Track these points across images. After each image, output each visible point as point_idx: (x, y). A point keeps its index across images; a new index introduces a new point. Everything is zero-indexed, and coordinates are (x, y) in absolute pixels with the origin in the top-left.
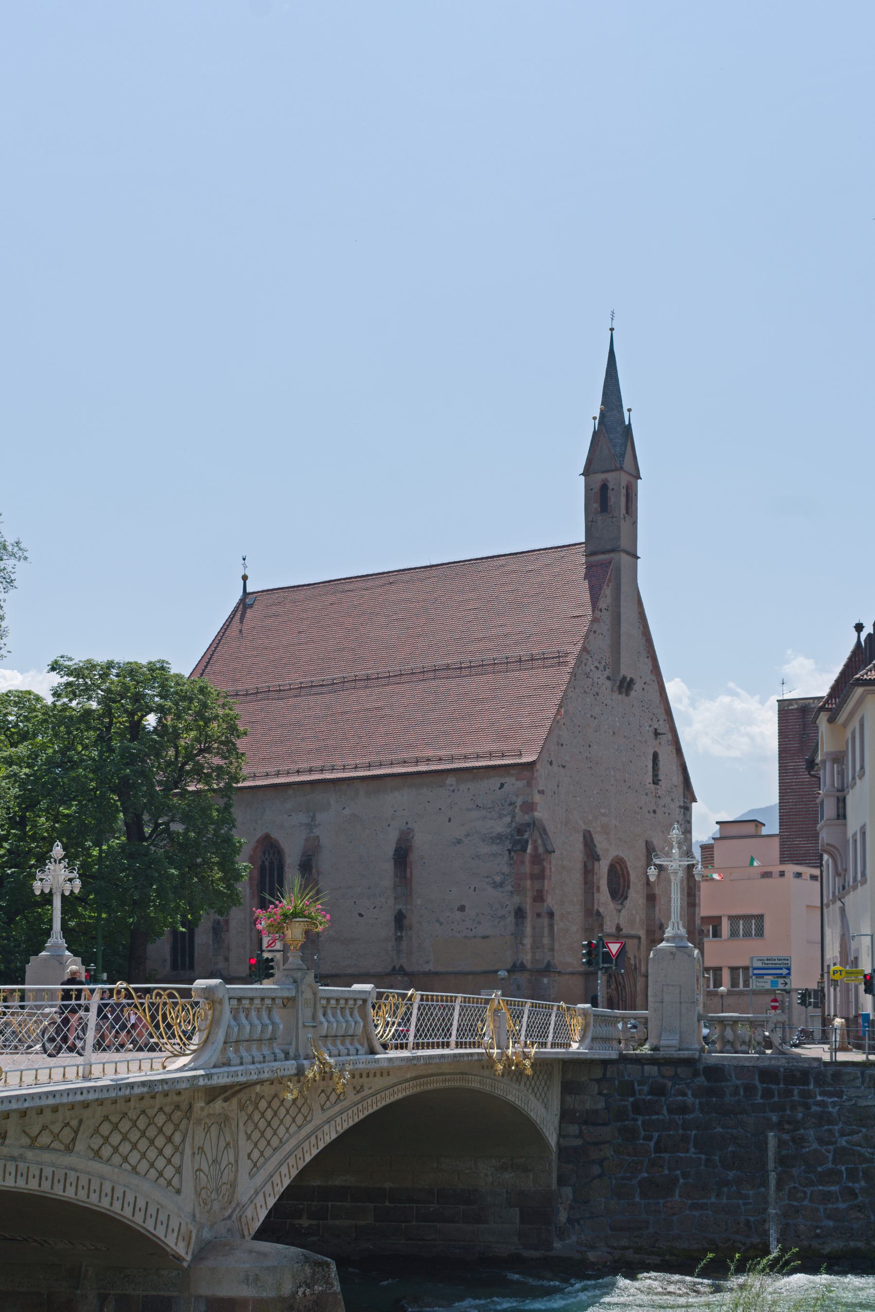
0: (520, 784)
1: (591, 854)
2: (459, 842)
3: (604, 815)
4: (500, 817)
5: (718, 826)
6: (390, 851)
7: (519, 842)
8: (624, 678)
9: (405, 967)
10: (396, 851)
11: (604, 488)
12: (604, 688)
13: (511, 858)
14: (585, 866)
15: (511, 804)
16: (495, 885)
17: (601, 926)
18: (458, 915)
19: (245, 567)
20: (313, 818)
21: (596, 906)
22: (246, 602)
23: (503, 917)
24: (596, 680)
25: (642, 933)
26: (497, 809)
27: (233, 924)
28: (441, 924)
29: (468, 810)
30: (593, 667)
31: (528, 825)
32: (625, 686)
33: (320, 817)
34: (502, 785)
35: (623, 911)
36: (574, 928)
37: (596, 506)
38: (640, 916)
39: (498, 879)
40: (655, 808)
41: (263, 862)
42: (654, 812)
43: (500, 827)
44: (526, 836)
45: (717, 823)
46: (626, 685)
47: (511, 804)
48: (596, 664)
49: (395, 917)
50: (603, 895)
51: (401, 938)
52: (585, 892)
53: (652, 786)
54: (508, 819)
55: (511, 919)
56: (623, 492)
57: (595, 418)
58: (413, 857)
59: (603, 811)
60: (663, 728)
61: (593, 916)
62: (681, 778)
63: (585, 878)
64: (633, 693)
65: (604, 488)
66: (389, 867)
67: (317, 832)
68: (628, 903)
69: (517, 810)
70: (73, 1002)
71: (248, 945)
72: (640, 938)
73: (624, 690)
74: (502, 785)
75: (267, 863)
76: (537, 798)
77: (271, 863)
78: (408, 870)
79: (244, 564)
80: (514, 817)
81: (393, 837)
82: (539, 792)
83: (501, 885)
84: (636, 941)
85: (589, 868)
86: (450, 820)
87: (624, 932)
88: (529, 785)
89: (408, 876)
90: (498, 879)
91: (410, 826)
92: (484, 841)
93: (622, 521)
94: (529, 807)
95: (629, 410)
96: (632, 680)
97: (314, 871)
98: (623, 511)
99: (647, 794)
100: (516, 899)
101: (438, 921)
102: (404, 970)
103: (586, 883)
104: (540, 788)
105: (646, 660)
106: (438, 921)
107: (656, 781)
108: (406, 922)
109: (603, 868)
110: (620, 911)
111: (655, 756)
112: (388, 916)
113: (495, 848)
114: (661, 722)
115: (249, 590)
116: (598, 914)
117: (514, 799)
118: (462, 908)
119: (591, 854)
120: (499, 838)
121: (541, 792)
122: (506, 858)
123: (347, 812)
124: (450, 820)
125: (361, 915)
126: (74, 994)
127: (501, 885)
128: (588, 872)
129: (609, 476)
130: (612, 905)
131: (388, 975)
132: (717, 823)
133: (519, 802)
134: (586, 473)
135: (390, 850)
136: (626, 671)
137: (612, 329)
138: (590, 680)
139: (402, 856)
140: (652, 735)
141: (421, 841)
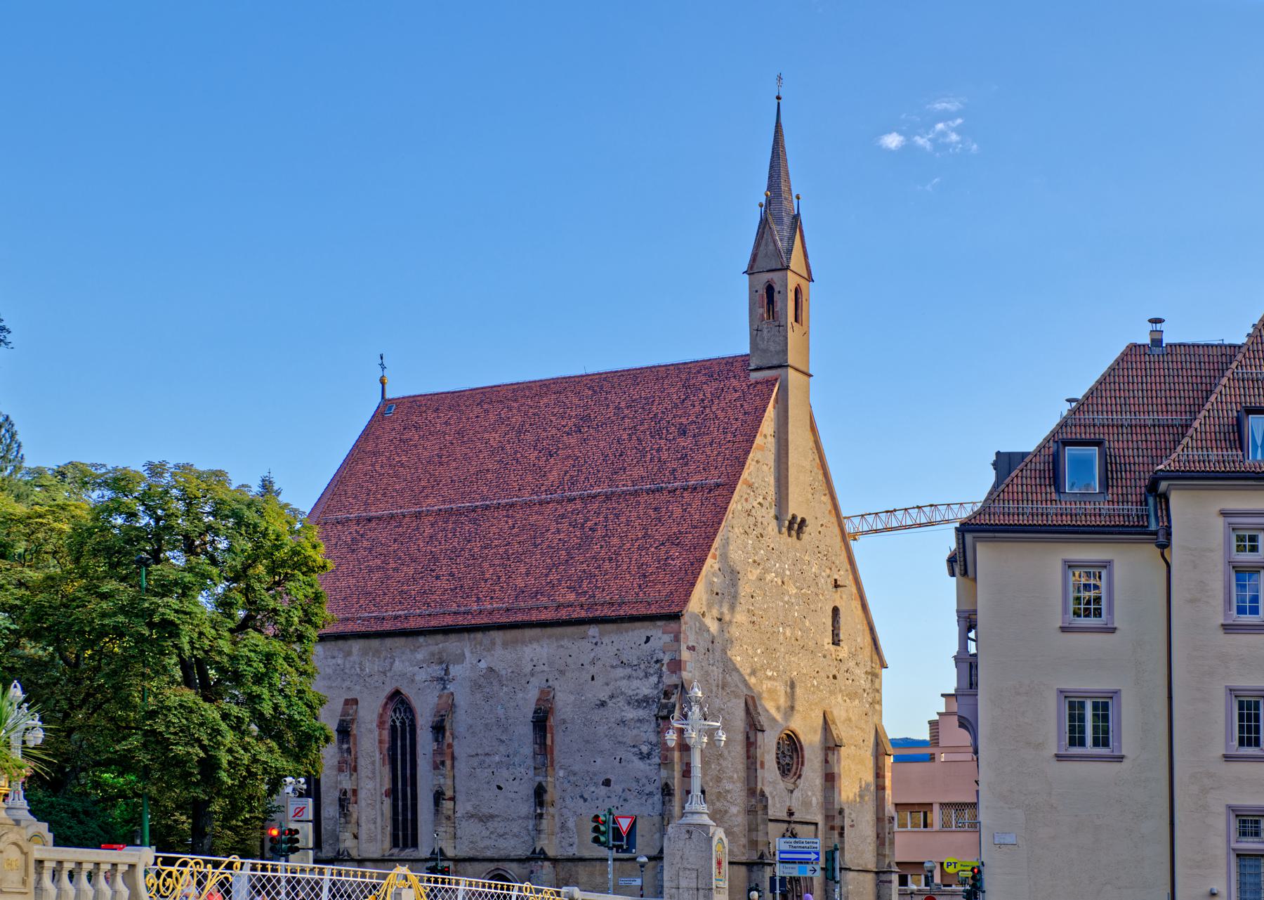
0: (667, 638)
1: (753, 726)
2: (603, 704)
3: (770, 678)
4: (646, 676)
5: (943, 699)
6: (531, 715)
7: (665, 706)
8: (794, 517)
9: (546, 849)
10: (535, 712)
11: (770, 289)
12: (770, 528)
13: (658, 725)
14: (748, 738)
15: (657, 662)
16: (643, 757)
17: (766, 807)
18: (603, 790)
19: (383, 367)
20: (447, 671)
21: (759, 786)
22: (380, 416)
23: (650, 794)
24: (760, 520)
25: (819, 819)
26: (642, 666)
27: (362, 794)
28: (585, 800)
29: (612, 667)
30: (755, 504)
31: (676, 686)
32: (797, 527)
33: (455, 670)
34: (648, 639)
35: (795, 792)
36: (734, 810)
37: (762, 311)
38: (816, 799)
39: (645, 749)
40: (835, 672)
41: (394, 721)
42: (835, 677)
43: (646, 688)
44: (672, 700)
45: (943, 695)
46: (796, 526)
47: (657, 662)
48: (760, 500)
49: (535, 792)
50: (769, 774)
51: (541, 816)
52: (748, 768)
53: (832, 648)
54: (654, 679)
55: (658, 797)
56: (791, 296)
57: (761, 206)
58: (552, 721)
59: (769, 673)
60: (844, 577)
61: (756, 798)
62: (868, 639)
63: (748, 751)
64: (805, 536)
65: (770, 289)
66: (525, 730)
67: (451, 687)
68: (801, 782)
69: (664, 669)
70: (343, 878)
71: (379, 820)
72: (816, 824)
73: (794, 533)
74: (648, 639)
75: (398, 724)
76: (685, 655)
77: (403, 723)
78: (549, 735)
79: (382, 364)
80: (660, 677)
81: (533, 695)
82: (689, 648)
83: (649, 755)
84: (813, 827)
85: (752, 740)
86: (593, 679)
87: (796, 817)
88: (677, 639)
89: (549, 742)
90: (645, 749)
91: (550, 683)
92: (629, 703)
93: (790, 331)
94: (676, 665)
95: (798, 198)
96: (803, 521)
97: (448, 734)
98: (791, 318)
99: (825, 657)
100: (664, 773)
101: (582, 797)
102: (544, 853)
103: (748, 757)
104: (690, 644)
105: (823, 498)
106: (582, 797)
107: (836, 642)
108: (547, 797)
109: (768, 745)
110: (792, 792)
111: (836, 611)
112: (527, 790)
113: (641, 713)
114: (842, 572)
115: (389, 396)
116: (763, 794)
117: (661, 655)
118: (607, 783)
119: (753, 726)
120: (644, 702)
121: (692, 648)
122: (653, 725)
123: (483, 665)
124: (593, 679)
125: (499, 788)
126: (269, 867)
127: (649, 755)
128: (750, 744)
129: (775, 276)
130: (782, 785)
131: (528, 859)
132: (943, 695)
133: (666, 660)
134: (750, 272)
135: (529, 700)
136: (796, 507)
137: (778, 98)
138: (752, 520)
139: (541, 722)
140: (830, 586)
141: (564, 703)
